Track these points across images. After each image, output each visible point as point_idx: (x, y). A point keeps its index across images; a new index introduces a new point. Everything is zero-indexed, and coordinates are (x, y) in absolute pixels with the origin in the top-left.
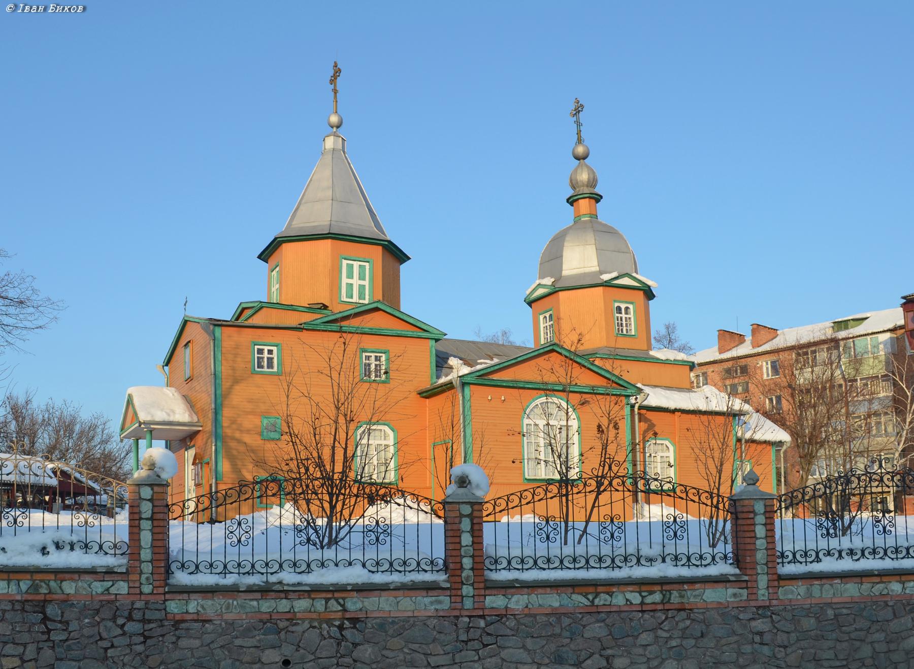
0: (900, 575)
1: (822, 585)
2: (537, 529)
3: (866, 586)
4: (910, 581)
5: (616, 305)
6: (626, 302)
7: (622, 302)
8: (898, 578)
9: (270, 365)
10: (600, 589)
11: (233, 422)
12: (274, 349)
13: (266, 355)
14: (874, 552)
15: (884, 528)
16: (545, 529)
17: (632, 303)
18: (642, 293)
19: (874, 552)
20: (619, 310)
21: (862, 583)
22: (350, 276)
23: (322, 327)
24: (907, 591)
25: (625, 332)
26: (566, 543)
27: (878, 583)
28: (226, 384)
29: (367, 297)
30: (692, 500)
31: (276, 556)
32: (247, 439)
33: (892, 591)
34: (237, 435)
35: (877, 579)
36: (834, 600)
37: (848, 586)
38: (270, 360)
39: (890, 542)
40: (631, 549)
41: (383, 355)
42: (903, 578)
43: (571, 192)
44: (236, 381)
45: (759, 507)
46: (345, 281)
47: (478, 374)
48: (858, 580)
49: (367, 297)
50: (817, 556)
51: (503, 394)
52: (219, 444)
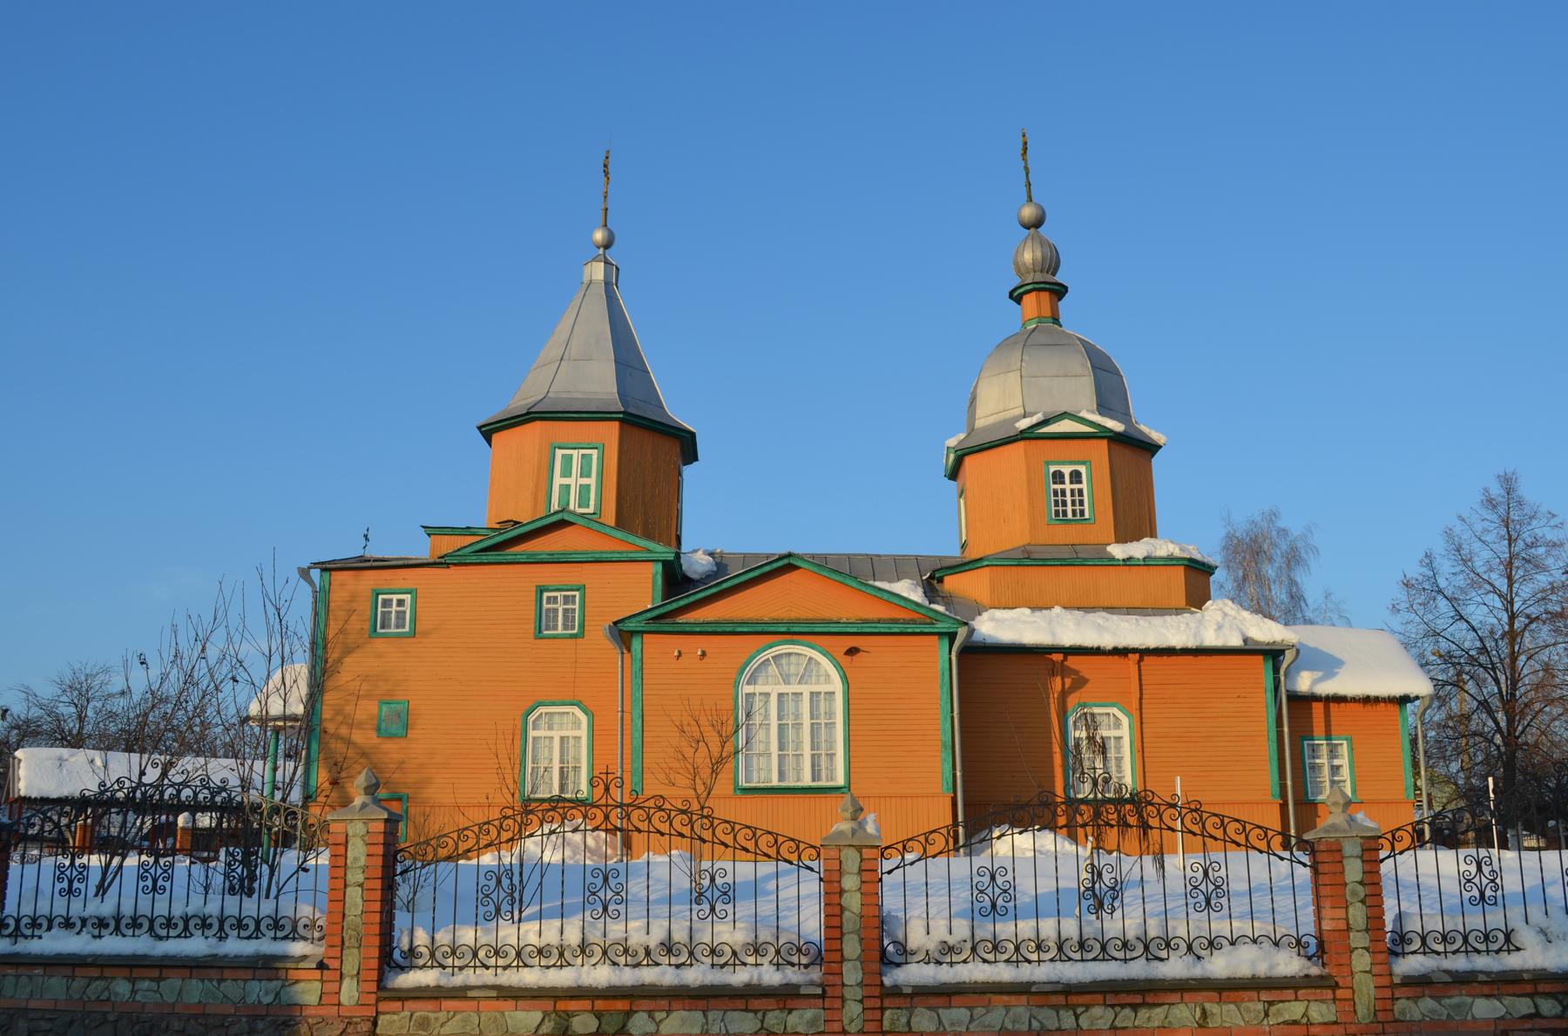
0: (131, 967)
1: (17, 977)
2: (1189, 888)
3: (230, 988)
4: (144, 979)
5: (1053, 469)
6: (1071, 463)
7: (1063, 463)
8: (126, 972)
9: (400, 625)
10: (227, 974)
11: (339, 712)
12: (407, 597)
13: (395, 607)
14: (135, 923)
15: (155, 881)
16: (1203, 887)
17: (1083, 463)
18: (1105, 442)
19: (205, 924)
20: (1058, 478)
21: (73, 977)
22: (566, 472)
23: (474, 559)
24: (138, 998)
25: (1070, 515)
26: (267, 897)
27: (97, 979)
28: (333, 656)
29: (592, 503)
30: (1170, 829)
31: (46, 911)
32: (357, 737)
33: (117, 994)
34: (344, 731)
35: (95, 972)
36: (33, 1004)
37: (53, 981)
38: (401, 615)
39: (161, 908)
40: (127, 909)
41: (577, 594)
42: (136, 972)
43: (1017, 281)
44: (348, 651)
45: (1351, 849)
46: (558, 480)
47: (649, 615)
48: (67, 971)
49: (592, 503)
50: (257, 928)
51: (698, 644)
52: (315, 746)
